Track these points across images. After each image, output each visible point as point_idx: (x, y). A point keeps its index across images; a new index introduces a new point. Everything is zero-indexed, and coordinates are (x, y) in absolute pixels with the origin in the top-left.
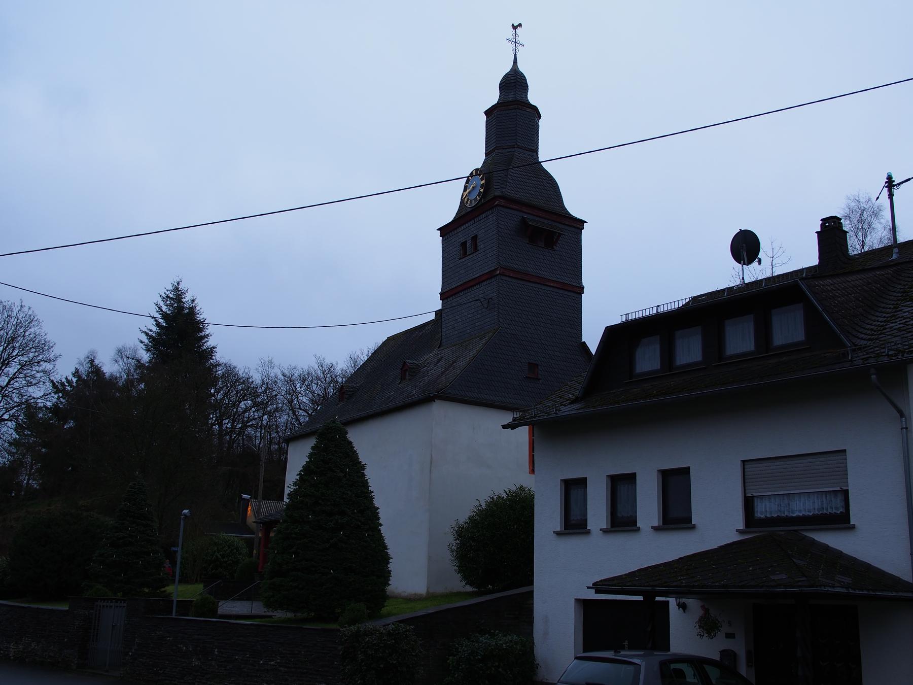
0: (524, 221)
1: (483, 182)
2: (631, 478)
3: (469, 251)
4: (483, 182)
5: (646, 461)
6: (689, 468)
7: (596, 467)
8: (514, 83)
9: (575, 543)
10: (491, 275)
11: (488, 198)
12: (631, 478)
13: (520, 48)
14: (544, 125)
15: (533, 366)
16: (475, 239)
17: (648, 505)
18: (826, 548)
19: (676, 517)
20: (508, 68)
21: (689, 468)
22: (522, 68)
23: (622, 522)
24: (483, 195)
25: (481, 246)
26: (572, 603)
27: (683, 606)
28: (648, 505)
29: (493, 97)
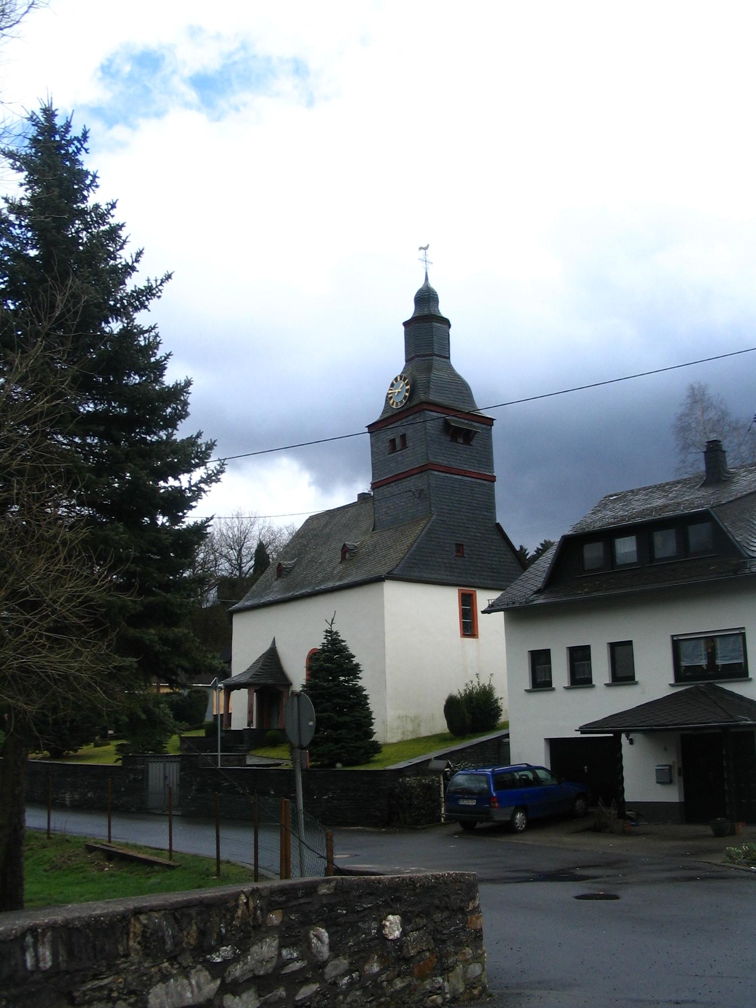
0: (446, 423)
1: (408, 387)
2: (546, 653)
3: (398, 447)
4: (408, 387)
5: (598, 635)
6: (589, 646)
7: (559, 639)
8: (426, 298)
9: (542, 697)
10: (422, 470)
11: (414, 403)
12: (546, 653)
13: (429, 266)
14: (455, 334)
15: (459, 547)
16: (403, 437)
17: (600, 667)
18: (732, 694)
19: (623, 674)
20: (420, 284)
21: (589, 646)
22: (433, 284)
23: (580, 678)
24: (409, 399)
25: (410, 444)
26: (543, 741)
27: (631, 742)
28: (600, 667)
29: (408, 311)
